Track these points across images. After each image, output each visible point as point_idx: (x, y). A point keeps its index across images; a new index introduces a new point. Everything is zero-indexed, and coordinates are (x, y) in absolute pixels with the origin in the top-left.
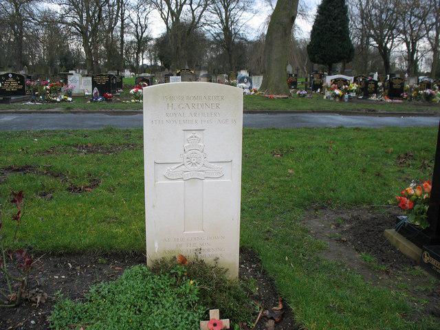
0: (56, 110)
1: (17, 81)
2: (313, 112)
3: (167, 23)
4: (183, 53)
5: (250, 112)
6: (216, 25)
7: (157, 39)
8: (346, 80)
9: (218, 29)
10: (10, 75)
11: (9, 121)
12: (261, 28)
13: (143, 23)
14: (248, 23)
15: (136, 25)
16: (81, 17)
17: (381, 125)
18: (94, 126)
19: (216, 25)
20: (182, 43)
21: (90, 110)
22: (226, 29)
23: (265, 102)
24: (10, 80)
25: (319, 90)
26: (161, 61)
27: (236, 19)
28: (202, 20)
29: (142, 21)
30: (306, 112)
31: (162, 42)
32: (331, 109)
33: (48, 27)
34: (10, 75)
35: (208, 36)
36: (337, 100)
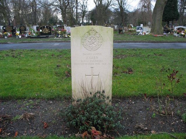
0: (25, 41)
1: (48, 29)
2: (179, 42)
3: (96, 3)
4: (100, 16)
5: (116, 42)
6: (117, 5)
7: (90, 11)
8: (183, 28)
9: (117, 7)
10: (45, 27)
11: (57, 45)
12: (137, 7)
13: (85, 5)
14: (130, 4)
15: (82, 6)
16: (60, 3)
17: (153, 48)
18: (145, 48)
19: (117, 5)
20: (103, 13)
21: (124, 41)
22: (121, 7)
23: (154, 38)
24: (45, 29)
25: (169, 33)
26: (91, 20)
27: (125, 2)
28: (111, 3)
29: (85, 3)
30: (176, 42)
31: (93, 13)
32: (139, 41)
33: (45, 8)
34: (45, 27)
35: (112, 10)
36: (182, 37)
